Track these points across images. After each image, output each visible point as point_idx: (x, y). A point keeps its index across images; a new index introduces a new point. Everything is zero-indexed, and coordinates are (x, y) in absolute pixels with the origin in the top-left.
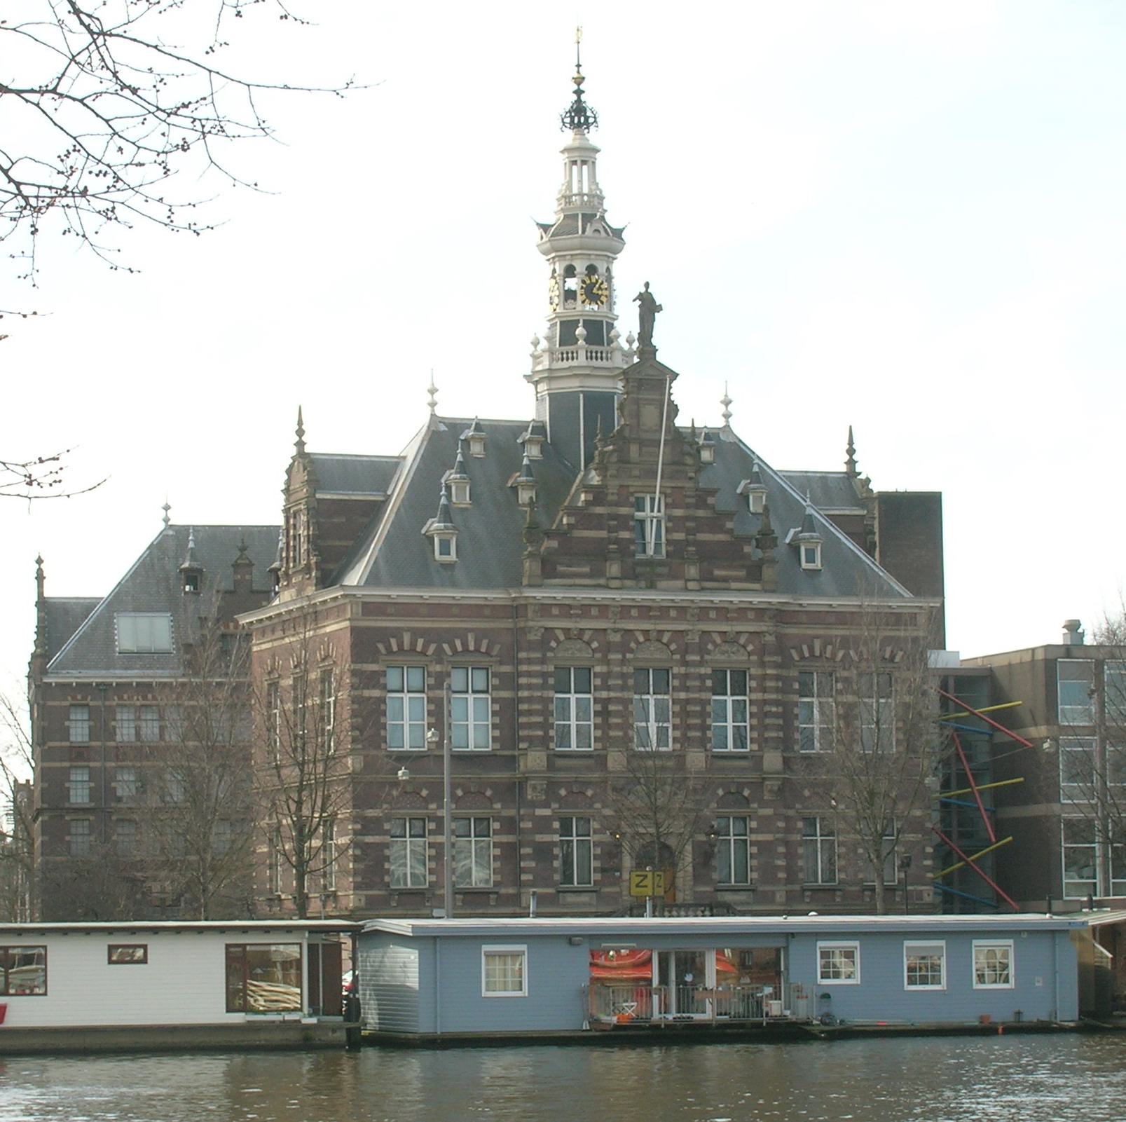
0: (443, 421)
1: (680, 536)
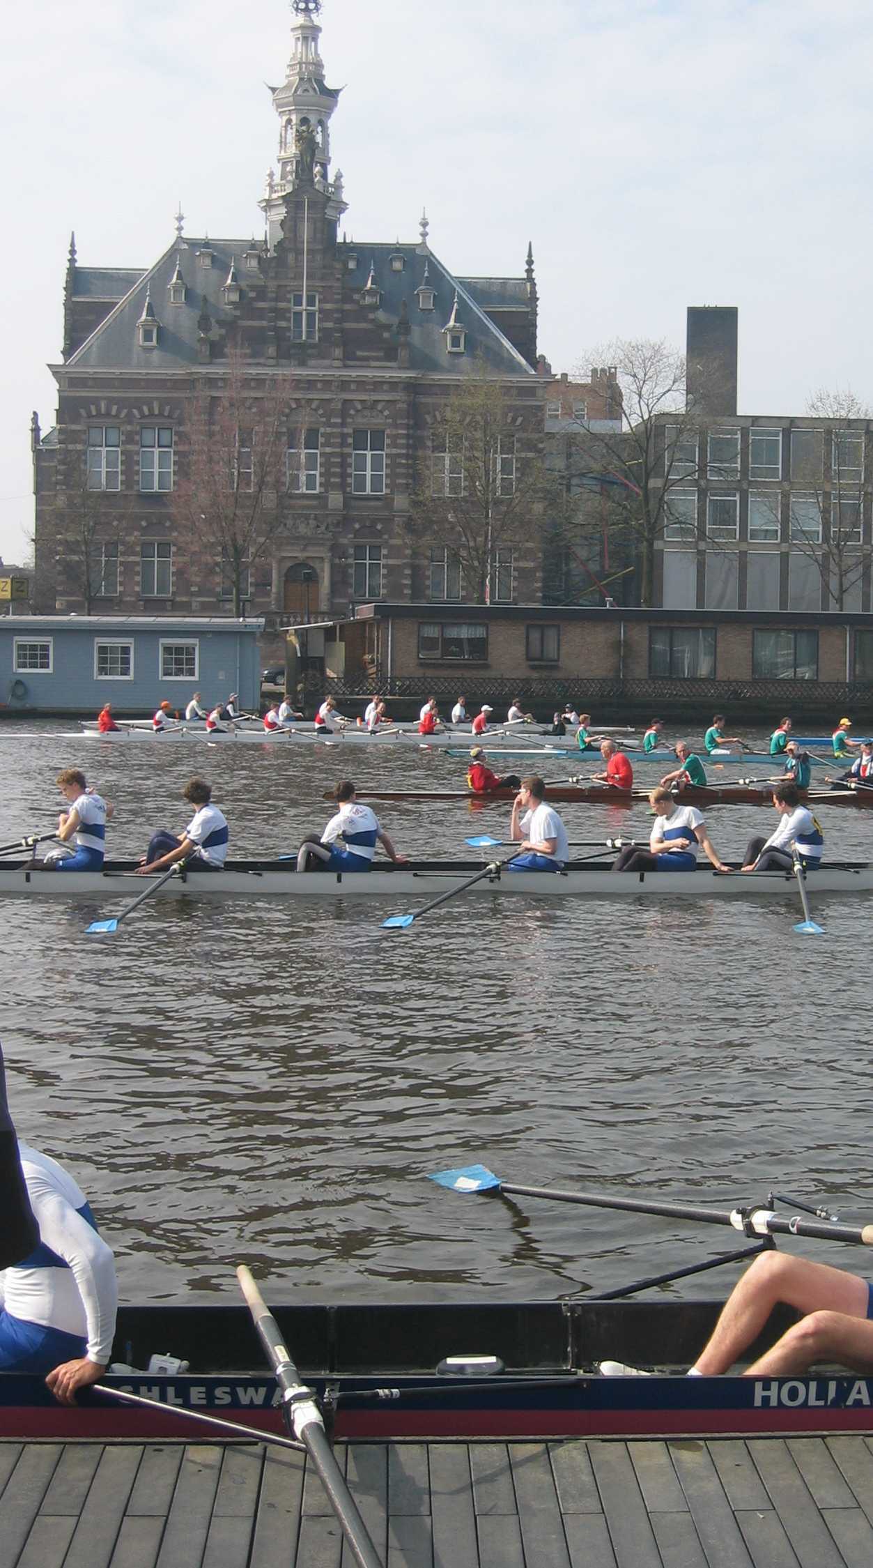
0: (186, 241)
1: (330, 325)
